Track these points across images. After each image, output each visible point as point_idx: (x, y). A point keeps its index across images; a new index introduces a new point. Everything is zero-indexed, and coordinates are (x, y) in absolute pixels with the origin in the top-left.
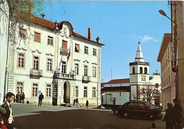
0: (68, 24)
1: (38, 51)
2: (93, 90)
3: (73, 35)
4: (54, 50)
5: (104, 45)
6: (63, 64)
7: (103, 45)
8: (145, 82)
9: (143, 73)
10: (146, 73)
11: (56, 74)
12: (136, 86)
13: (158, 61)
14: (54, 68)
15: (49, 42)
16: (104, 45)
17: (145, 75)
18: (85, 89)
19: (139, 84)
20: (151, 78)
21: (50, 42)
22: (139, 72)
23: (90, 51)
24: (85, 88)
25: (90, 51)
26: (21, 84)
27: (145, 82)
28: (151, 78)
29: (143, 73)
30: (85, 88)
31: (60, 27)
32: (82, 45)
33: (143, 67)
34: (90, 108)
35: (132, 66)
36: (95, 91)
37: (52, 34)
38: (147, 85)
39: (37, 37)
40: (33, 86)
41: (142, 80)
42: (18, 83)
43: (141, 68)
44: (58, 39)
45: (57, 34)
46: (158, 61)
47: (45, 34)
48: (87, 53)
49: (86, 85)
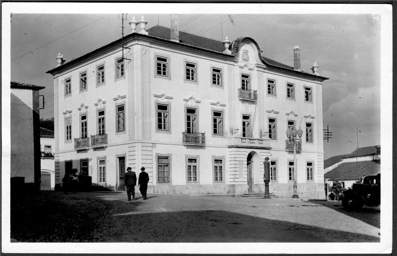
2: (216, 165)
3: (270, 65)
5: (328, 79)
6: (189, 114)
7: (326, 79)
15: (160, 69)
16: (328, 79)
18: (218, 165)
21: (216, 77)
23: (300, 93)
25: (300, 93)
26: (220, 162)
31: (235, 47)
32: (281, 80)
36: (104, 168)
39: (190, 73)
42: (160, 158)
44: (231, 73)
47: (205, 65)
48: (294, 98)
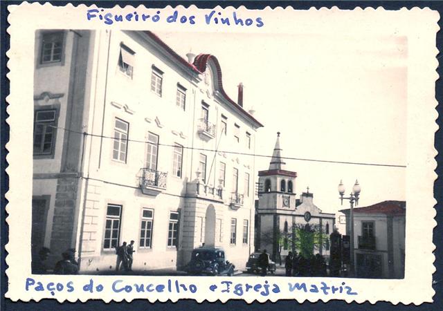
0: (214, 59)
1: (126, 108)
4: (189, 120)
8: (287, 208)
9: (286, 191)
10: (291, 191)
11: (192, 186)
12: (272, 216)
13: (403, 204)
14: (185, 172)
17: (288, 196)
19: (278, 212)
20: (298, 203)
22: (279, 190)
24: (147, 213)
27: (287, 208)
28: (298, 203)
29: (286, 191)
30: (147, 213)
33: (287, 180)
34: (112, 269)
35: (265, 178)
37: (185, 82)
38: (272, 214)
40: (144, 216)
41: (284, 205)
43: (283, 182)
45: (193, 82)
46: (403, 204)
49: (148, 202)
